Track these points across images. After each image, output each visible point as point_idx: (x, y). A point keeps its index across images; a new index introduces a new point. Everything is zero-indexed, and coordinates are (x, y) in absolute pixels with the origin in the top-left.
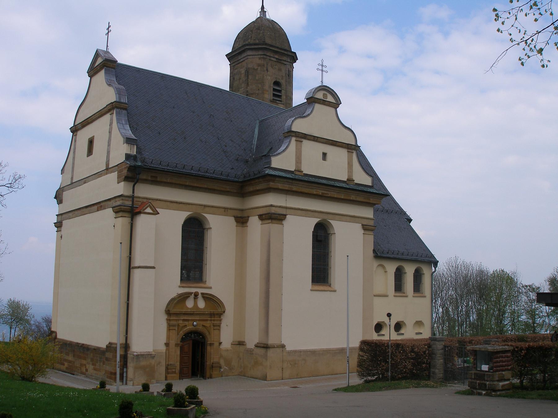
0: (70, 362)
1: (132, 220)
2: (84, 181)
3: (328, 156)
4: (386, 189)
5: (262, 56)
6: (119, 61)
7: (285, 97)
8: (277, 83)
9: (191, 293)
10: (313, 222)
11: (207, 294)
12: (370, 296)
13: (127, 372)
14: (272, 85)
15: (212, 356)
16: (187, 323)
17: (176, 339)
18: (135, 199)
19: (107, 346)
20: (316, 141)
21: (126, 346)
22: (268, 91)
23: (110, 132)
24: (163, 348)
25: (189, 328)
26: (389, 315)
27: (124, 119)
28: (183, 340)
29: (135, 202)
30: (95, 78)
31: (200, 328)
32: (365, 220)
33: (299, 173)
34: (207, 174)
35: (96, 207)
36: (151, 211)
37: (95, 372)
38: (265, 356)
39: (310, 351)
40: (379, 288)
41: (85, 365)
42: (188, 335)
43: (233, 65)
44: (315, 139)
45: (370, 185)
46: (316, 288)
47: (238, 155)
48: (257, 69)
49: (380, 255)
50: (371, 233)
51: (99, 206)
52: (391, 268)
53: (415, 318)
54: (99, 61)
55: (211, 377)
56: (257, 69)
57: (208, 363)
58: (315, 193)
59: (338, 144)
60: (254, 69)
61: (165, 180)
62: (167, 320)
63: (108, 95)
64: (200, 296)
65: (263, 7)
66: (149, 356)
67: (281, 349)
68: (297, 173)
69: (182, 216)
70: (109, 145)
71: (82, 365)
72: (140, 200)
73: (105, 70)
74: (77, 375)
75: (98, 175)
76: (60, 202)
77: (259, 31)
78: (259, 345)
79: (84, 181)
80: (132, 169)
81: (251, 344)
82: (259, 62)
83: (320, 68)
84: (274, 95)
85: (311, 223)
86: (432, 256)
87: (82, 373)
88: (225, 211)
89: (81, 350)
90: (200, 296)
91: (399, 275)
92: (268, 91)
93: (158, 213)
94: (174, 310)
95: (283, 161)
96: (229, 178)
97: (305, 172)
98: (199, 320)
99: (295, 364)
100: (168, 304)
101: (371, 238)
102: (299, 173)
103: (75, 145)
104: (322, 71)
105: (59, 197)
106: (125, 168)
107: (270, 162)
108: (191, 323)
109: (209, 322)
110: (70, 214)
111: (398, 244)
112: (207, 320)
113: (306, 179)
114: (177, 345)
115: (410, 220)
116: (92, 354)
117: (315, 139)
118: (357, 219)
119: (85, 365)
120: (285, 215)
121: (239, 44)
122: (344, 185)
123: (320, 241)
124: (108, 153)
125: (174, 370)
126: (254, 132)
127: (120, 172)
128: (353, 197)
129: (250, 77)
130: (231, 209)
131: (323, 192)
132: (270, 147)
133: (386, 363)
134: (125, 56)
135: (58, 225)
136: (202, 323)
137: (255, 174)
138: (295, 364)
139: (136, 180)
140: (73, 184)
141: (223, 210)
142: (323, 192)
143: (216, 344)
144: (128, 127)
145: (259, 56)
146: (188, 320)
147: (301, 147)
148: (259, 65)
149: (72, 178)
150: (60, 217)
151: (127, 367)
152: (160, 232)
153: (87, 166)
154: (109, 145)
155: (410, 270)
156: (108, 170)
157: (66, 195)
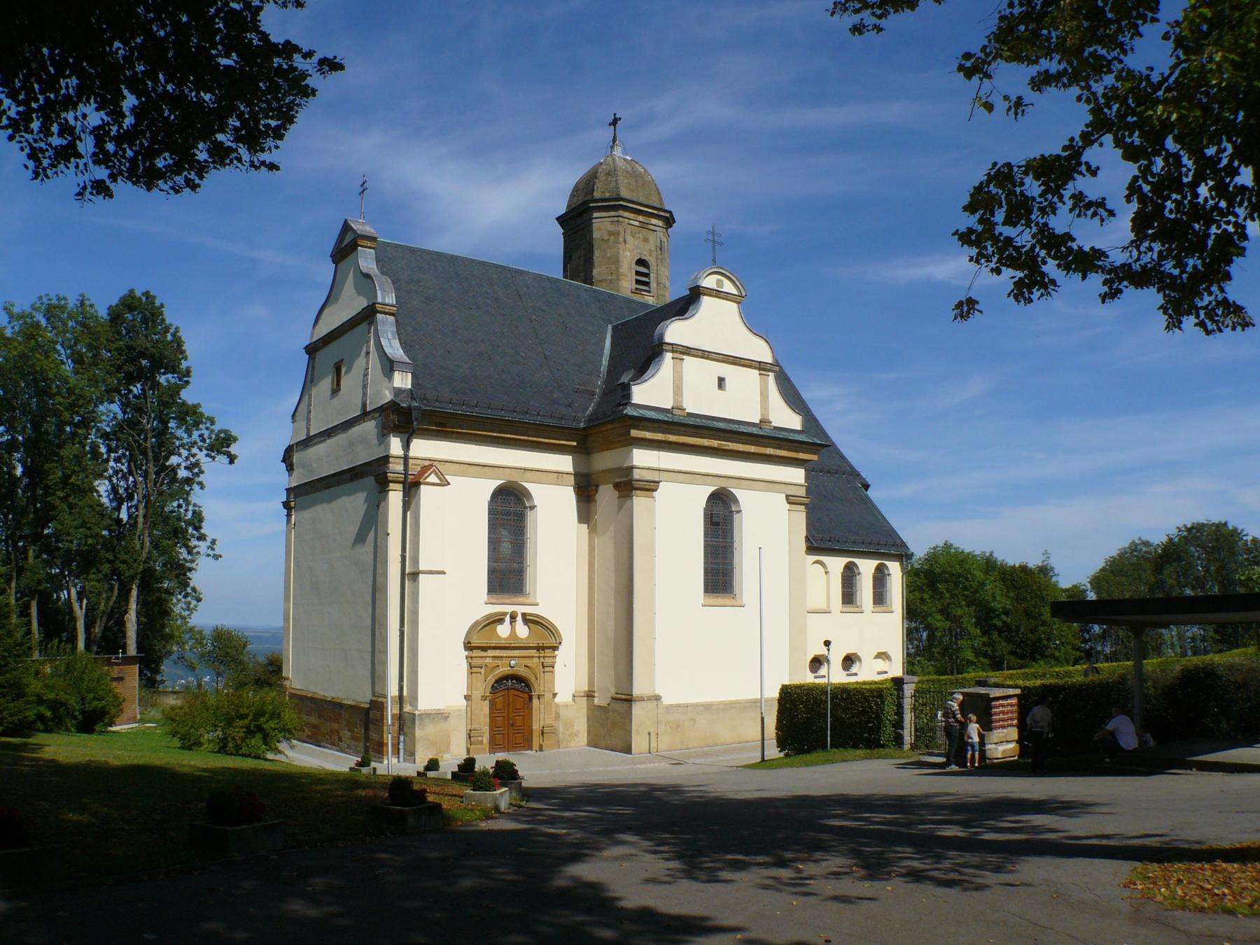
0: (314, 726)
3: (728, 383)
4: (826, 436)
8: (641, 262)
9: (505, 614)
11: (531, 615)
12: (800, 612)
14: (634, 266)
15: (540, 717)
16: (499, 662)
17: (483, 688)
18: (411, 461)
20: (707, 358)
25: (504, 670)
26: (827, 643)
31: (521, 671)
42: (500, 681)
46: (847, 609)
49: (819, 543)
52: (837, 564)
64: (519, 618)
68: (676, 412)
76: (290, 468)
82: (611, 228)
83: (717, 238)
84: (638, 282)
87: (333, 744)
90: (519, 618)
91: (850, 576)
94: (478, 644)
97: (690, 409)
100: (469, 633)
101: (801, 517)
103: (313, 374)
105: (288, 458)
108: (506, 661)
109: (535, 660)
113: (691, 421)
114: (484, 698)
115: (867, 487)
122: (755, 431)
123: (717, 524)
124: (365, 387)
129: (597, 253)
140: (308, 442)
143: (548, 696)
148: (611, 233)
149: (308, 430)
156: (365, 415)
157: (296, 458)
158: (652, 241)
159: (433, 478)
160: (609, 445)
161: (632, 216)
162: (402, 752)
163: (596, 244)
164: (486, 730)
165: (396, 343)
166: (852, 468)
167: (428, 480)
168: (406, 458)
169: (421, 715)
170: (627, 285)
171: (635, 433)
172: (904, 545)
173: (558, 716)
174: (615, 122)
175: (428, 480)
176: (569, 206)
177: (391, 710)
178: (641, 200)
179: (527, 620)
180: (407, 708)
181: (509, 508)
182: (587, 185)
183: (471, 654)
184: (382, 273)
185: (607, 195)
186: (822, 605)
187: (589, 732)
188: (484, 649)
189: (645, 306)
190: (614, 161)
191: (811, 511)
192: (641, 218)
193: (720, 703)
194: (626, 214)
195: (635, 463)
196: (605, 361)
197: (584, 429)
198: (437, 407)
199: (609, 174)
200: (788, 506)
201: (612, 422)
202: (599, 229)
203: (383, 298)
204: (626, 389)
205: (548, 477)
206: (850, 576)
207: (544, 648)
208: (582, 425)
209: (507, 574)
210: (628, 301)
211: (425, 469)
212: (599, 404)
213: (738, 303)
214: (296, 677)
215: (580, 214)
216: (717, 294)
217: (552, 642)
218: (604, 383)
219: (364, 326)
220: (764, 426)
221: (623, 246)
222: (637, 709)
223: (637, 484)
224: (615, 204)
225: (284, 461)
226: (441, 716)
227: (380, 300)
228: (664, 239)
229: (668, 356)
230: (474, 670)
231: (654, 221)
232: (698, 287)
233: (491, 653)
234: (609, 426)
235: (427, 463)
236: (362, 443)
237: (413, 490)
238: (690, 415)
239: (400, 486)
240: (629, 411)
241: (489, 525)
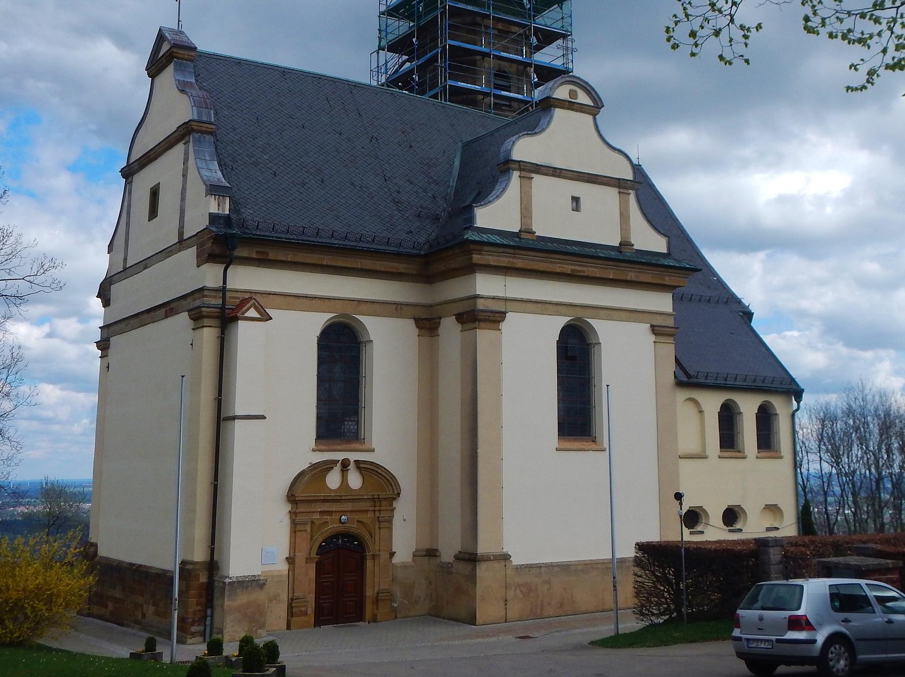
1: (223, 332)
2: (145, 264)
6: (201, 47)
9: (335, 462)
10: (557, 323)
11: (365, 462)
12: (669, 457)
13: (212, 616)
15: (375, 582)
18: (228, 294)
20: (559, 176)
21: (213, 566)
23: (185, 176)
24: (283, 567)
25: (333, 526)
27: (208, 150)
28: (321, 550)
29: (228, 299)
30: (159, 79)
31: (354, 528)
32: (657, 317)
33: (528, 236)
34: (361, 244)
35: (162, 311)
36: (257, 315)
38: (472, 578)
40: (688, 442)
41: (142, 606)
42: (330, 540)
45: (665, 251)
46: (726, 454)
47: (421, 207)
49: (687, 379)
50: (671, 340)
51: (168, 309)
52: (712, 402)
53: (756, 495)
54: (165, 47)
55: (374, 620)
57: (369, 593)
58: (558, 270)
61: (283, 258)
62: (290, 512)
63: (178, 109)
67: (503, 563)
68: (524, 235)
69: (315, 322)
70: (183, 199)
73: (176, 63)
74: (128, 626)
75: (167, 253)
79: (145, 264)
80: (218, 239)
81: (447, 555)
85: (552, 327)
86: (793, 380)
87: (136, 622)
88: (395, 309)
90: (352, 467)
91: (728, 418)
94: (304, 493)
95: (496, 215)
96: (401, 249)
97: (540, 233)
98: (351, 511)
101: (669, 350)
102: (528, 236)
103: (130, 201)
105: (104, 294)
106: (209, 239)
107: (471, 219)
110: (122, 325)
111: (724, 359)
112: (367, 511)
113: (540, 245)
114: (308, 560)
118: (641, 315)
120: (505, 313)
122: (613, 254)
123: (573, 358)
125: (303, 609)
126: (452, 165)
127: (200, 247)
128: (631, 276)
130: (407, 305)
131: (573, 267)
132: (477, 192)
133: (694, 582)
134: (207, 41)
135: (103, 345)
136: (358, 517)
141: (394, 306)
142: (573, 267)
143: (384, 556)
144: (215, 165)
146: (330, 513)
149: (125, 260)
150: (106, 330)
151: (212, 607)
153: (152, 236)
154: (183, 199)
155: (748, 407)
156: (182, 243)
157: (115, 289)
159: (252, 313)
167: (246, 315)
171: (476, 258)
175: (246, 315)
186: (694, 448)
193: (579, 563)
211: (244, 302)
216: (570, 105)
217: (390, 494)
220: (625, 250)
222: (483, 571)
226: (254, 583)
229: (516, 175)
235: (247, 296)
236: (189, 273)
240: (470, 235)
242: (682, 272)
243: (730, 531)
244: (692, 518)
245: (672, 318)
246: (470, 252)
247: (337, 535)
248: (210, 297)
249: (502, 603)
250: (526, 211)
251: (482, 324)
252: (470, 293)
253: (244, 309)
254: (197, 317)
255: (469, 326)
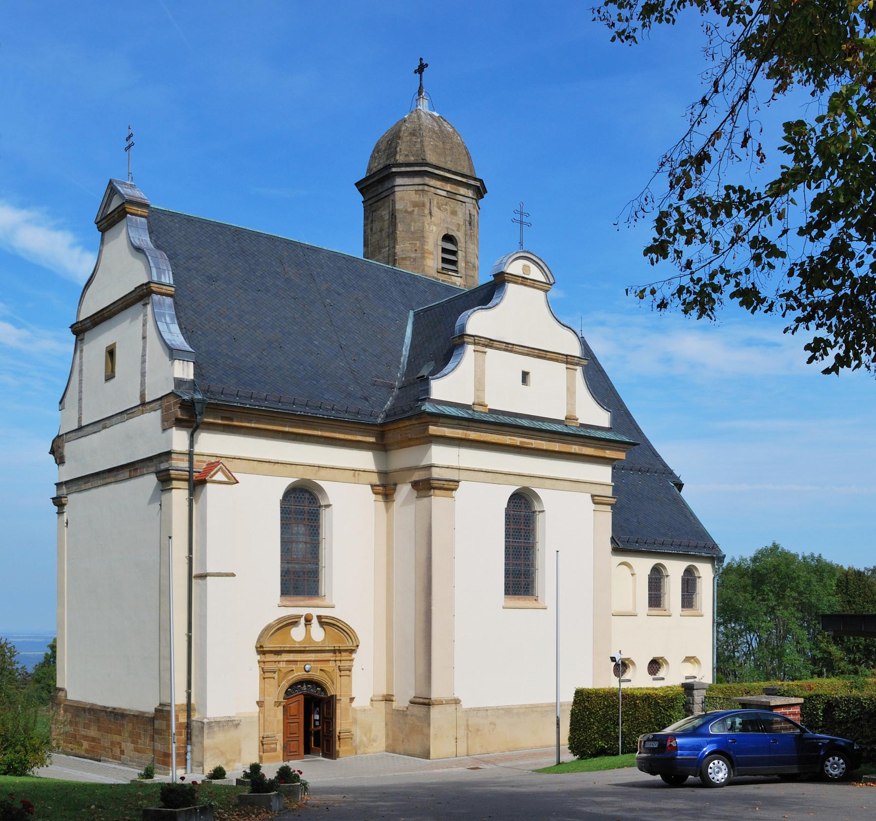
0: (93, 739)
2: (103, 423)
3: (532, 378)
5: (420, 187)
7: (463, 265)
8: (448, 238)
9: (300, 617)
11: (326, 617)
14: (440, 242)
16: (293, 667)
17: (276, 693)
18: (195, 458)
19: (156, 710)
20: (511, 351)
22: (432, 253)
25: (299, 674)
29: (195, 463)
31: (317, 675)
37: (137, 754)
38: (427, 717)
39: (503, 709)
41: (119, 743)
42: (295, 686)
43: (370, 202)
44: (508, 347)
48: (412, 212)
49: (624, 544)
51: (133, 469)
52: (644, 565)
54: (115, 203)
56: (412, 212)
59: (549, 355)
60: (406, 211)
64: (315, 621)
65: (748, 89)
66: (230, 724)
68: (477, 408)
70: (143, 362)
71: (113, 744)
72: (205, 458)
74: (105, 761)
75: (127, 414)
76: (60, 460)
77: (414, 139)
78: (417, 700)
79: (103, 423)
80: (188, 406)
81: (401, 702)
82: (415, 197)
83: (525, 219)
84: (444, 260)
87: (114, 757)
89: (112, 718)
90: (315, 621)
91: (656, 579)
92: (432, 253)
93: (237, 482)
99: (478, 730)
100: (261, 636)
101: (606, 517)
104: (521, 223)
105: (57, 451)
107: (427, 391)
108: (300, 666)
109: (332, 664)
114: (277, 704)
115: (680, 486)
116: (130, 725)
117: (508, 347)
119: (119, 743)
121: (379, 164)
124: (143, 374)
125: (273, 746)
129: (400, 227)
137: (404, 412)
138: (478, 730)
139: (195, 425)
140: (81, 430)
145: (416, 187)
147: (484, 361)
148: (415, 204)
152: (242, 515)
156: (144, 405)
157: (69, 449)
158: (460, 214)
159: (220, 476)
160: (407, 443)
161: (438, 184)
162: (189, 762)
163: (399, 216)
164: (280, 737)
165: (175, 328)
166: (665, 466)
167: (214, 478)
168: (191, 454)
169: (209, 723)
170: (432, 264)
171: (433, 430)
172: (715, 547)
173: (355, 721)
174: (421, 69)
175: (214, 478)
176: (369, 170)
177: (177, 719)
178: (449, 166)
179: (323, 622)
180: (195, 717)
181: (302, 507)
182: (390, 144)
183: (263, 658)
184: (158, 247)
185: (412, 159)
187: (387, 736)
188: (278, 653)
189: (449, 289)
190: (419, 117)
191: (616, 510)
192: (449, 187)
193: (521, 707)
194: (433, 182)
195: (435, 461)
196: (405, 351)
197: (381, 425)
198: (221, 399)
199: (413, 134)
200: (593, 506)
201: (409, 418)
202: (402, 199)
203: (159, 277)
204: (424, 382)
205: (344, 471)
206: (656, 579)
207: (340, 651)
208: (379, 421)
209: (301, 575)
210: (433, 284)
211: (211, 466)
212: (397, 398)
213: (546, 291)
214: (76, 683)
215: (381, 181)
216: (523, 281)
217: (349, 645)
218: (405, 375)
219: (139, 305)
221: (428, 218)
222: (435, 711)
223: (435, 484)
224: (421, 170)
225: (52, 452)
226: (232, 724)
227: (155, 279)
228: (474, 212)
229: (470, 349)
230: (267, 675)
231: (463, 191)
232: (503, 273)
233: (285, 657)
234: (407, 423)
235: (213, 460)
236: (148, 435)
237: (198, 488)
238: (492, 411)
239: (185, 485)
240: (428, 407)
241: (282, 519)
242: (622, 446)
243: (654, 679)
244: (621, 667)
245: (611, 488)
246: (427, 424)
247: (302, 682)
248: (178, 460)
249: (454, 741)
250: (479, 385)
251: (437, 492)
252: (424, 463)
253: (212, 473)
254: (165, 480)
255: (423, 493)
